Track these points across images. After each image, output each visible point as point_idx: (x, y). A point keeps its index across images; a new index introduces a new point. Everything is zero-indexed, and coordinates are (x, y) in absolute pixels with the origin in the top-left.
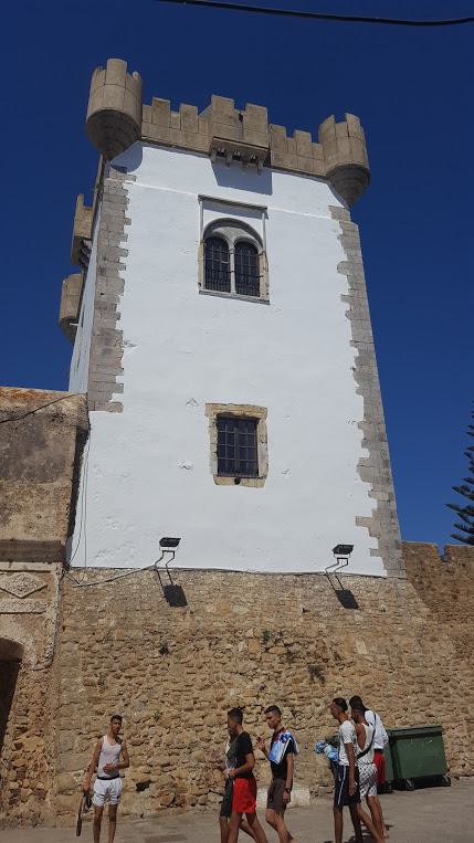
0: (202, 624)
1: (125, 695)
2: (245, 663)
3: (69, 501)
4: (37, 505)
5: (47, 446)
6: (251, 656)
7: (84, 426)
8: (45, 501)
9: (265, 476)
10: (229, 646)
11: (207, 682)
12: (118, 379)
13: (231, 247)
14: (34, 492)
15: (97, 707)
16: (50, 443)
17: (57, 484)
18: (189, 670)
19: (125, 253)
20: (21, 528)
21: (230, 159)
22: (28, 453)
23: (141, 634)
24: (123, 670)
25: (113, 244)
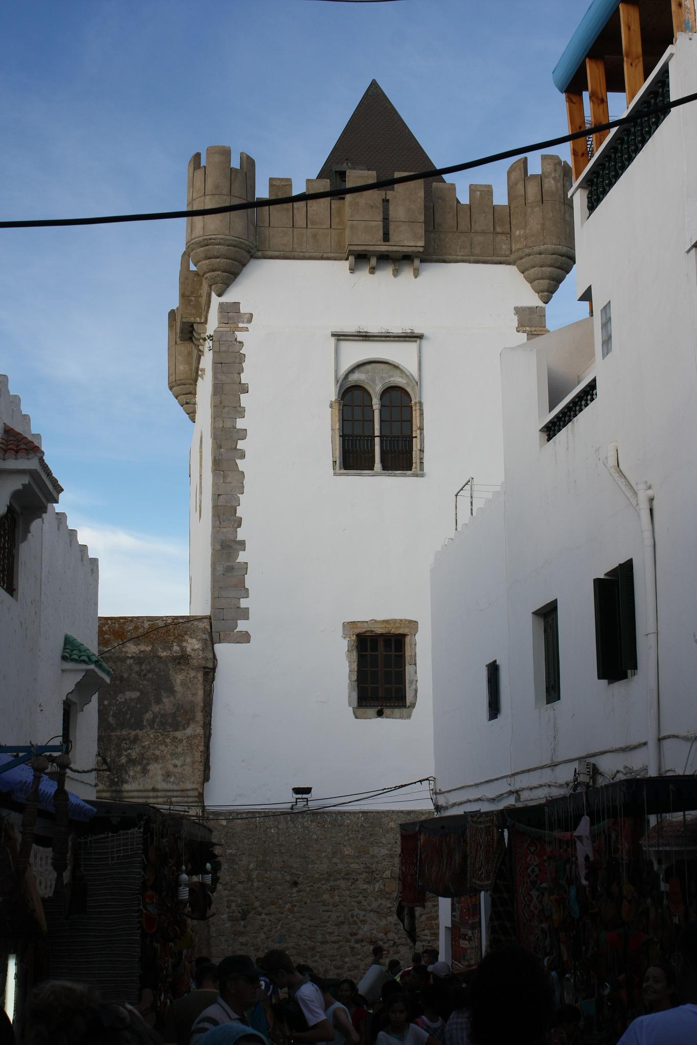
0: (339, 866)
1: (265, 929)
2: (380, 901)
3: (202, 748)
4: (172, 755)
5: (175, 691)
6: (388, 896)
7: (184, 348)
8: (180, 749)
9: (413, 705)
10: (366, 886)
11: (340, 919)
12: (244, 603)
13: (376, 404)
14: (168, 741)
15: (242, 939)
16: (178, 688)
17: (189, 731)
18: (325, 908)
19: (243, 434)
20: (160, 778)
21: (373, 261)
22: (159, 701)
23: (279, 876)
24: (263, 908)
25: (228, 424)
